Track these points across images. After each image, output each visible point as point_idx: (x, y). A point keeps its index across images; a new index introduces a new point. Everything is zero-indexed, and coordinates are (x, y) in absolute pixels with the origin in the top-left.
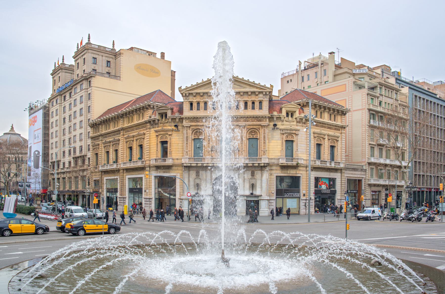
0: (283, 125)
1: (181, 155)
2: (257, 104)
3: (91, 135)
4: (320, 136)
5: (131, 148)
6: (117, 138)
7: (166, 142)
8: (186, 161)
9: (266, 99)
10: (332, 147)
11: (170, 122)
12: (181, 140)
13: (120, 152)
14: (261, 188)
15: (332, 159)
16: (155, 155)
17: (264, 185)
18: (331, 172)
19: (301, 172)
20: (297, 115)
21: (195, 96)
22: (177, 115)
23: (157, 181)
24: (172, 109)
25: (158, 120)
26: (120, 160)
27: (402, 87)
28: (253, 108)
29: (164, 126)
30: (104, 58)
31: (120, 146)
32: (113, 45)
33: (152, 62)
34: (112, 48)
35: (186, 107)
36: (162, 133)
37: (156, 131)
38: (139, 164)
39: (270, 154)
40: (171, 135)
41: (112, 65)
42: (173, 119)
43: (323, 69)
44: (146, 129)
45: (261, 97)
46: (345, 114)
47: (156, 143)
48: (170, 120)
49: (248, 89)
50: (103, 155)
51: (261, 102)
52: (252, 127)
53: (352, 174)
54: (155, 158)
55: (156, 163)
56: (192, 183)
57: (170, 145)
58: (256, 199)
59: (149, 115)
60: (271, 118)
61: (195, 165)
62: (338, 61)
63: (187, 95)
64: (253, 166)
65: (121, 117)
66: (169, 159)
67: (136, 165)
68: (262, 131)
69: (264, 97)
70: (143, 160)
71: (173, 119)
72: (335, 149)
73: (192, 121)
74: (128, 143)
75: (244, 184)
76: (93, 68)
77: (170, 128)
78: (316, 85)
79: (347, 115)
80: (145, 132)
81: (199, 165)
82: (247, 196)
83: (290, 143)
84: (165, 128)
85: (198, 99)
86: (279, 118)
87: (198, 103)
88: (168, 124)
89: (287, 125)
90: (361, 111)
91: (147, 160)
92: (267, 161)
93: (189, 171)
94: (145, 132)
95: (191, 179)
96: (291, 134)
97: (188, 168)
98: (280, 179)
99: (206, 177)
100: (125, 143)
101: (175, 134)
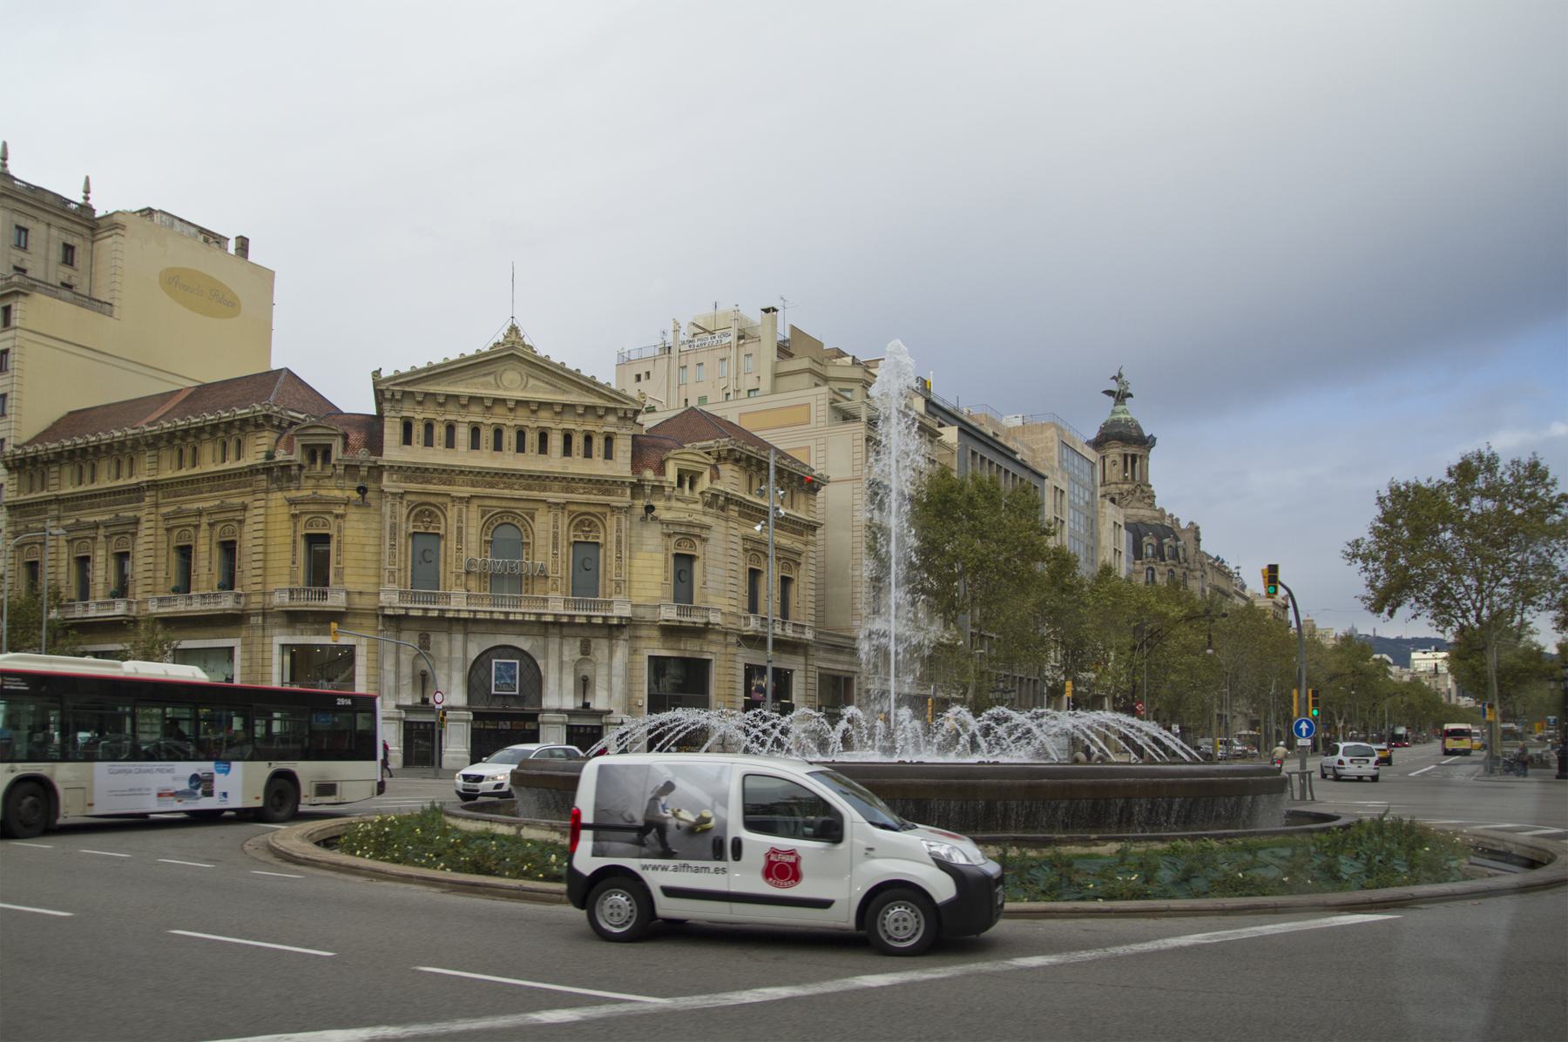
0: (669, 509)
1: (374, 580)
2: (598, 444)
3: (9, 495)
4: (755, 548)
5: (185, 552)
6: (131, 514)
7: (326, 539)
8: (391, 599)
9: (624, 431)
10: (786, 582)
11: (339, 477)
12: (374, 534)
13: (140, 562)
14: (610, 689)
15: (785, 614)
16: (287, 578)
17: (618, 683)
18: (784, 652)
19: (713, 648)
20: (704, 483)
21: (420, 403)
22: (362, 455)
23: (287, 658)
24: (346, 437)
25: (301, 467)
26: (139, 590)
27: (941, 425)
28: (498, 446)
29: (318, 487)
30: (54, 232)
31: (140, 541)
32: (87, 191)
33: (215, 271)
34: (81, 201)
35: (392, 433)
36: (312, 508)
37: (292, 502)
38: (227, 603)
39: (634, 592)
40: (342, 516)
41: (80, 257)
42: (352, 469)
43: (743, 351)
44: (254, 492)
45: (610, 424)
46: (816, 491)
47: (289, 540)
48: (340, 470)
49: (574, 397)
50: (64, 570)
51: (609, 439)
52: (584, 509)
53: (831, 661)
54: (287, 586)
55: (294, 603)
56: (406, 670)
57: (339, 549)
58: (594, 722)
59: (265, 448)
60: (637, 488)
61: (420, 613)
62: (784, 332)
63: (398, 396)
64: (589, 625)
65: (148, 445)
66: (338, 591)
67: (212, 607)
68: (611, 522)
69: (621, 424)
70: (238, 590)
71: (352, 469)
72: (793, 588)
73: (408, 479)
74: (176, 532)
75: (560, 680)
76: (15, 261)
77: (338, 493)
78: (722, 397)
79: (819, 494)
80: (248, 500)
81: (430, 614)
82: (571, 713)
83: (683, 564)
84: (323, 492)
85: (430, 413)
86: (658, 489)
87: (429, 426)
88: (332, 482)
89: (679, 510)
90: (849, 485)
91: (255, 593)
92: (626, 612)
93: (399, 631)
94: (248, 500)
95: (403, 657)
96: (688, 537)
97: (397, 621)
98: (658, 666)
99: (450, 652)
100: (160, 532)
101: (353, 515)
